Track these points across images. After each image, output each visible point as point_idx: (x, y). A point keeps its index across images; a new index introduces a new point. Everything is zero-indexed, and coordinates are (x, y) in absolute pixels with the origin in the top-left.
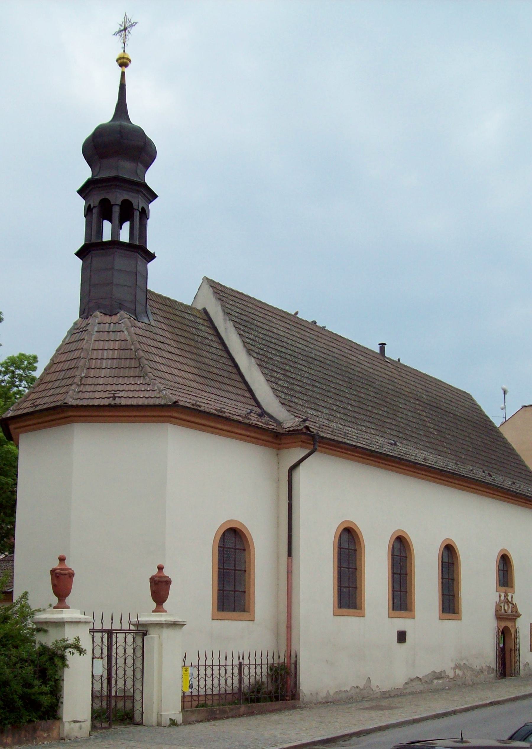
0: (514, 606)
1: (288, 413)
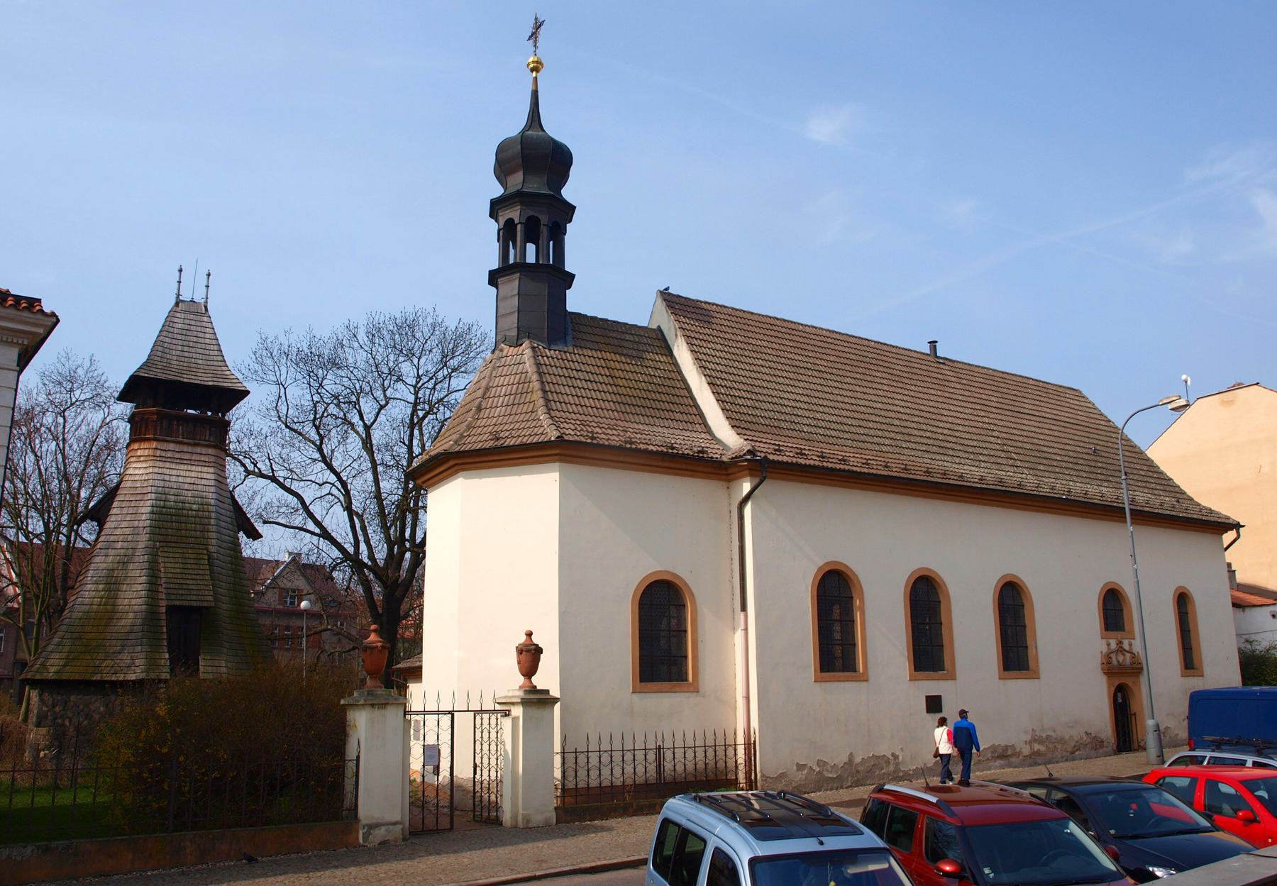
1: (738, 436)
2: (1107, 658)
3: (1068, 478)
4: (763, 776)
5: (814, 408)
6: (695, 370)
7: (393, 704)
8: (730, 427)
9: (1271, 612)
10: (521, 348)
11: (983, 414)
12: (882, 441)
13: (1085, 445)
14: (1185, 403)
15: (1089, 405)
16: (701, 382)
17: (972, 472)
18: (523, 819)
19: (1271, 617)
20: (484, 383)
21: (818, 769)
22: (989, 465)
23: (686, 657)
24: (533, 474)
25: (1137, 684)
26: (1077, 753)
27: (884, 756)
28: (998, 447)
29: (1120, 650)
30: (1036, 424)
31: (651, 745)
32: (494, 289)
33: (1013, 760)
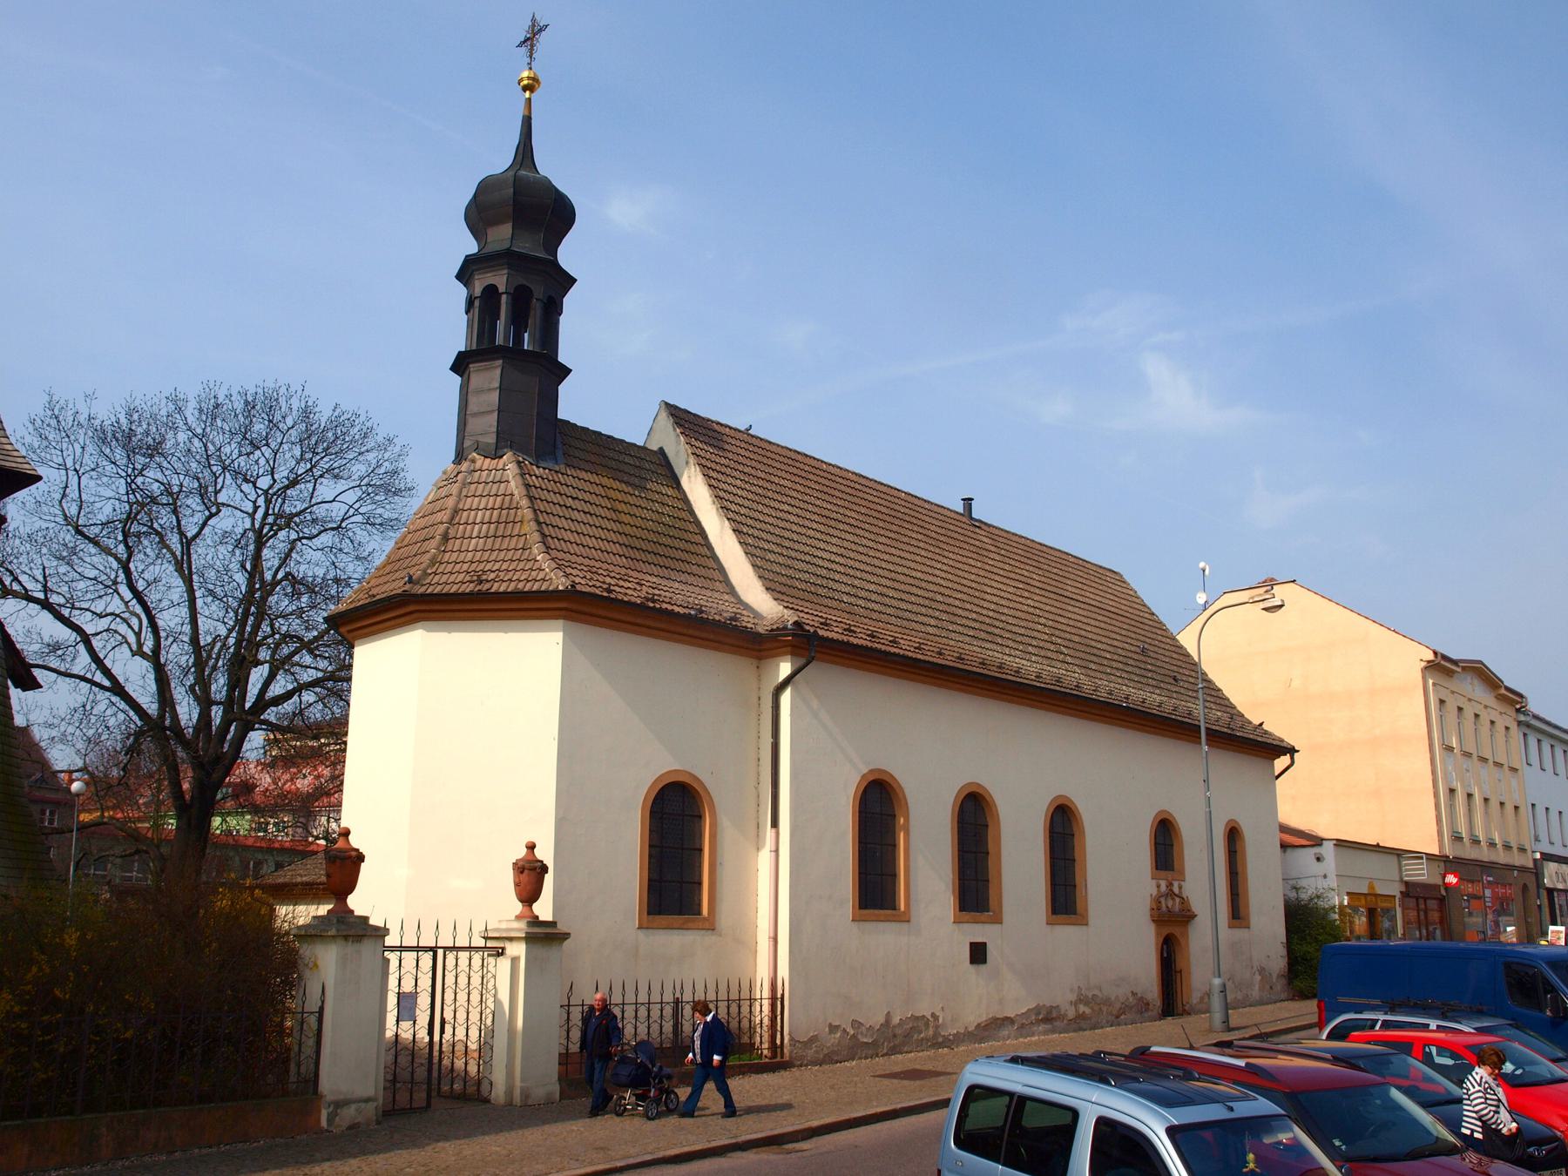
0: (1184, 901)
1: (775, 602)
2: (1157, 900)
3: (1120, 680)
4: (792, 1039)
5: (852, 572)
6: (715, 510)
7: (371, 936)
8: (763, 589)
9: (1315, 854)
10: (502, 461)
11: (1026, 594)
12: (926, 620)
13: (1132, 642)
14: (1280, 603)
15: (1131, 593)
16: (722, 528)
17: (1029, 667)
18: (521, 1094)
19: (1315, 861)
20: (450, 502)
21: (852, 1032)
22: (1040, 660)
23: (700, 884)
24: (474, 631)
25: (1185, 935)
26: (1122, 1017)
27: (924, 1016)
28: (1046, 637)
29: (1170, 894)
30: (1081, 612)
31: (668, 997)
32: (458, 379)
33: (1057, 1023)
